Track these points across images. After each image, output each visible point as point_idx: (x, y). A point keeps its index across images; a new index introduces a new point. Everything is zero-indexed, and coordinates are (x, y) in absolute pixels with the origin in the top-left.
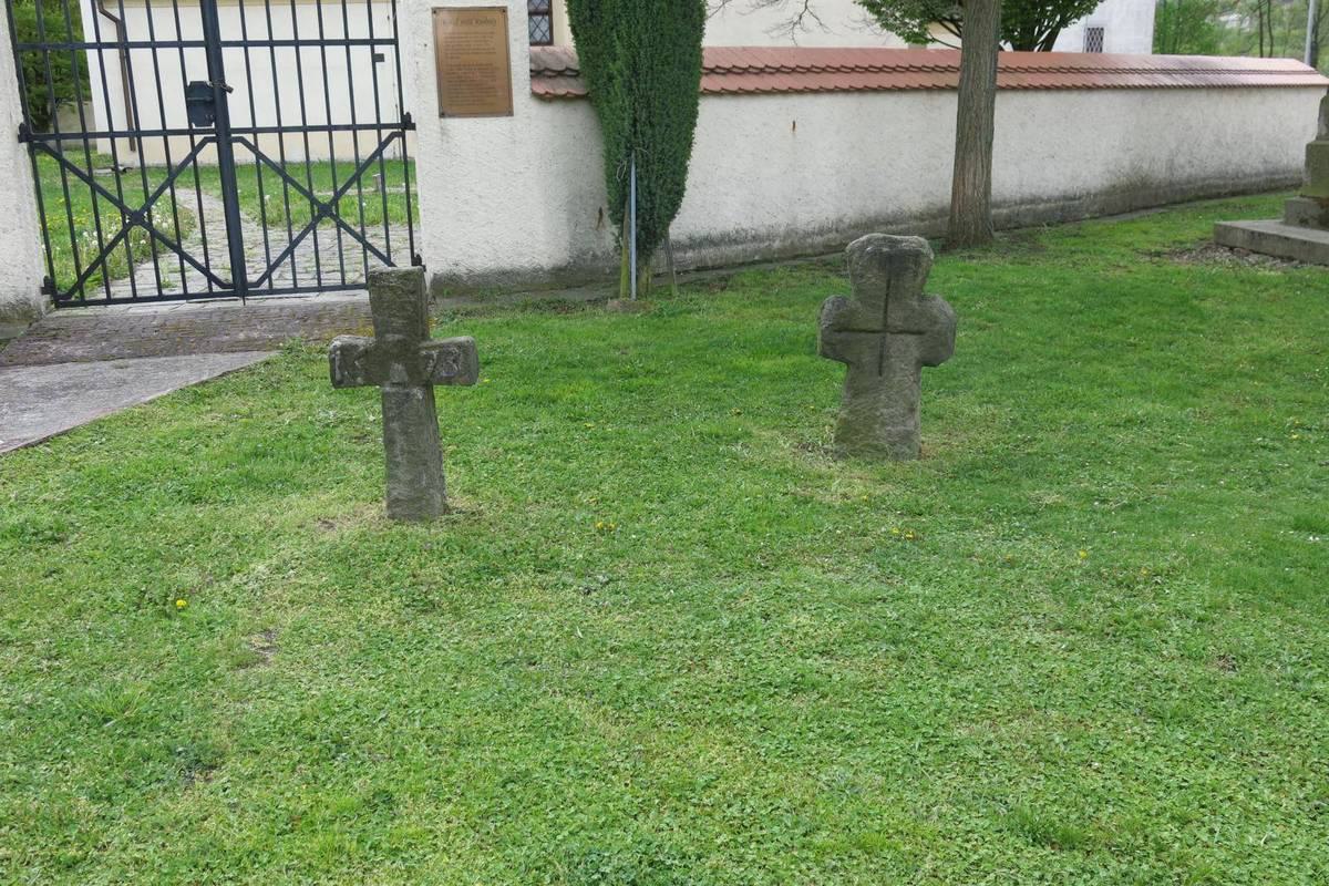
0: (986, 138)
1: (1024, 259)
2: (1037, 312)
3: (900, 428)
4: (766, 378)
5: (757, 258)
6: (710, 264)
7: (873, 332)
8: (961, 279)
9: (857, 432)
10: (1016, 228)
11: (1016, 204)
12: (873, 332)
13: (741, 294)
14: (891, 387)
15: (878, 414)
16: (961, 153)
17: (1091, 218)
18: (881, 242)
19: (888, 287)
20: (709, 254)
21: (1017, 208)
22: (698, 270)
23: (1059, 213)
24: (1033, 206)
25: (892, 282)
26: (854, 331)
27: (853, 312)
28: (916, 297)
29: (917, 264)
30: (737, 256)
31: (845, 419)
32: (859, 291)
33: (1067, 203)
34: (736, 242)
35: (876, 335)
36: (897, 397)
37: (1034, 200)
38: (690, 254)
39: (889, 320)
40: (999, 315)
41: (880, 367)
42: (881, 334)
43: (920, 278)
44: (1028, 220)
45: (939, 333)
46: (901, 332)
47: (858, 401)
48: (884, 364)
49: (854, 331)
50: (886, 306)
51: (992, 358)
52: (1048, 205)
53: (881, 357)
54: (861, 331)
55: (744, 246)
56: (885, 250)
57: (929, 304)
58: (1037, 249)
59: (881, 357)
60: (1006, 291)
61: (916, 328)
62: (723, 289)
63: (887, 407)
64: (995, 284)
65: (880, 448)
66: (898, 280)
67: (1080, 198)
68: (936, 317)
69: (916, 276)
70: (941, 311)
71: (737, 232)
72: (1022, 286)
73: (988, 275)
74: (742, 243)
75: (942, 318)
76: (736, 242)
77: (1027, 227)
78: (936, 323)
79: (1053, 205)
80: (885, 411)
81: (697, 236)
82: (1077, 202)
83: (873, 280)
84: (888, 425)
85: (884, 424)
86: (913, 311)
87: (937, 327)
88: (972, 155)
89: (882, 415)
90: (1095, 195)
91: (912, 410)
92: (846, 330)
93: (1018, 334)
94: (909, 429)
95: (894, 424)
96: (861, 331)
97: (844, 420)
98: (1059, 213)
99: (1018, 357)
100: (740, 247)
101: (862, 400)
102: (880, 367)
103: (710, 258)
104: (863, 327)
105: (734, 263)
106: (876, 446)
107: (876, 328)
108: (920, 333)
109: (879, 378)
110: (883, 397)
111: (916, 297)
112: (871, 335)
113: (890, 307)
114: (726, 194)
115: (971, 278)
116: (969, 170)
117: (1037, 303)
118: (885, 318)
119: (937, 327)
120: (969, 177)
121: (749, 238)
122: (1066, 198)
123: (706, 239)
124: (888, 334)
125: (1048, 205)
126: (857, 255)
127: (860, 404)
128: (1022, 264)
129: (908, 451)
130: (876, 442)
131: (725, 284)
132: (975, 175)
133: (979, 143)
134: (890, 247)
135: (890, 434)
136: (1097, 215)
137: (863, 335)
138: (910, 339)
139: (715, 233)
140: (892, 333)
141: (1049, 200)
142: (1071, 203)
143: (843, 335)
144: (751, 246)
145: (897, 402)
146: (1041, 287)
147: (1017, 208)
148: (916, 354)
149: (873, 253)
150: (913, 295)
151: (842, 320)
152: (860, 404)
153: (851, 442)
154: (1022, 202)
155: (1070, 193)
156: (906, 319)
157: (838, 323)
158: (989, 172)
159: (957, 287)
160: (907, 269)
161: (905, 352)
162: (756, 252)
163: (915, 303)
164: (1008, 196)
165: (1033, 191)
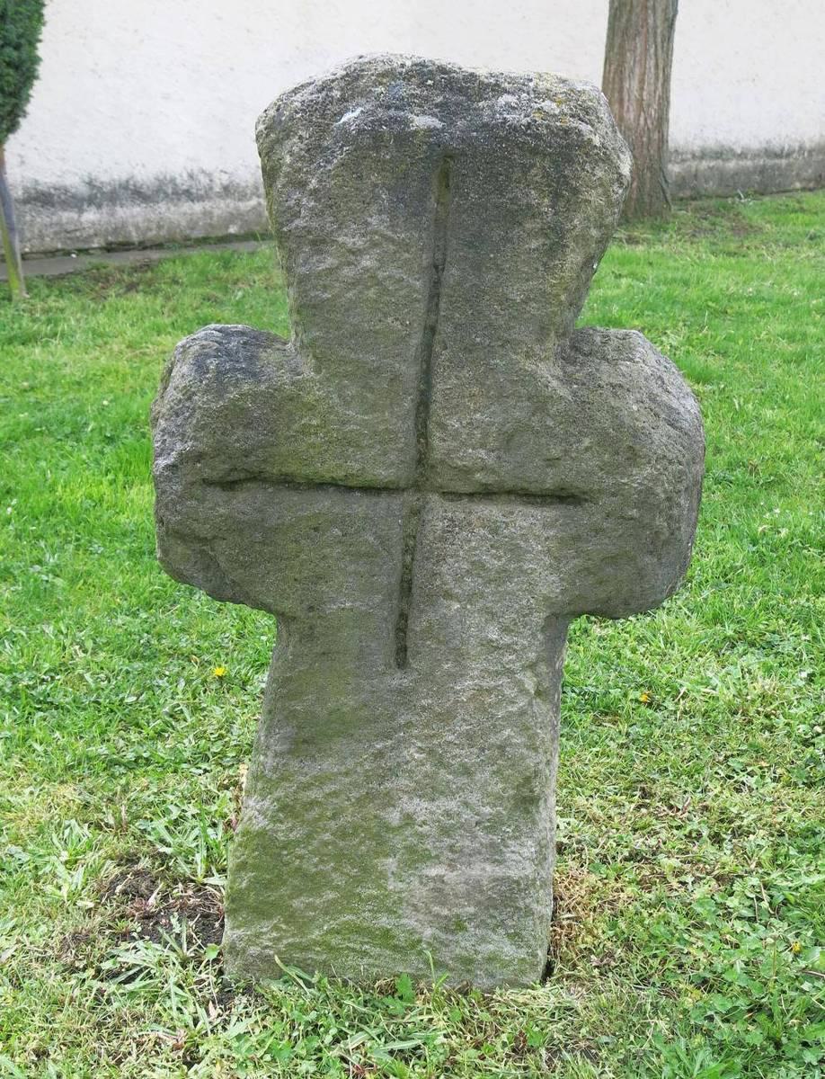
0: (665, 11)
1: (732, 247)
2: (800, 359)
3: (484, 871)
4: (122, 547)
5: (233, 230)
6: (135, 237)
7: (371, 489)
8: (624, 281)
9: (314, 883)
10: (694, 199)
11: (694, 156)
12: (371, 489)
13: (159, 300)
14: (446, 717)
15: (394, 817)
16: (618, 41)
17: (803, 189)
18: (405, 90)
19: (434, 296)
20: (133, 216)
21: (694, 164)
22: (109, 249)
23: (757, 178)
24: (720, 162)
25: (452, 273)
26: (288, 482)
27: (281, 404)
28: (552, 343)
29: (563, 191)
30: (193, 225)
31: (262, 834)
32: (308, 310)
33: (770, 162)
34: (189, 195)
35: (383, 501)
36: (469, 756)
37: (720, 154)
38: (90, 216)
39: (439, 444)
40: (715, 364)
41: (402, 629)
42: (410, 498)
43: (574, 258)
44: (711, 186)
45: (645, 499)
46: (487, 493)
47: (313, 769)
48: (418, 625)
49: (288, 482)
50: (427, 375)
51: (717, 481)
52: (742, 163)
53: (406, 587)
54: (321, 485)
55: (208, 205)
56: (421, 121)
57: (606, 374)
58: (744, 230)
59: (406, 587)
60: (719, 309)
61: (550, 481)
62: (131, 287)
63: (430, 790)
64: (693, 293)
65: (402, 938)
66: (478, 268)
67: (788, 155)
68: (635, 434)
69: (555, 248)
70: (655, 406)
71: (191, 176)
72: (750, 299)
73: (679, 275)
74: (200, 198)
75: (661, 436)
76: (189, 195)
77: (709, 197)
78: (634, 457)
79: (749, 163)
80: (419, 807)
81: (104, 178)
82: (784, 162)
83: (367, 262)
84: (426, 858)
85: (415, 857)
86: (540, 403)
87: (641, 475)
88: (639, 42)
89: (409, 819)
90: (810, 152)
91: (527, 802)
92: (256, 477)
93: (768, 414)
94: (514, 873)
95: (457, 857)
96: (321, 485)
97: (262, 842)
98: (757, 178)
99: (780, 481)
100: (198, 207)
101: (328, 765)
102: (402, 629)
103: (137, 227)
104: (329, 468)
105: (187, 239)
106: (387, 934)
107: (383, 474)
108: (563, 497)
109: (398, 680)
110: (413, 753)
111: (552, 343)
112: (360, 506)
113: (442, 386)
114: (166, 97)
115: (644, 280)
116: (632, 71)
117: (791, 338)
118: (422, 433)
119: (641, 475)
120: (632, 85)
121: (217, 189)
122: (769, 153)
123: (125, 186)
124: (434, 498)
125: (742, 163)
126: (294, 144)
127: (320, 781)
128: (729, 254)
129: (509, 950)
130: (384, 921)
131: (141, 280)
132: (642, 81)
133: (651, 21)
134: (445, 111)
135: (440, 892)
136: (811, 185)
137: (325, 503)
138: (527, 521)
139: (145, 175)
140: (452, 495)
141: (742, 156)
142: (777, 161)
143: (244, 503)
144: (221, 207)
145: (467, 771)
146: (787, 302)
147: (694, 164)
148: (549, 584)
149: (371, 140)
150: (543, 333)
151: (238, 439)
152: (320, 781)
153: (291, 918)
154: (703, 155)
155: (776, 145)
156: (508, 441)
157: (219, 450)
158: (667, 80)
159: (618, 297)
160: (514, 216)
161: (503, 576)
162: (232, 218)
163: (548, 372)
164: (682, 143)
165: (720, 137)
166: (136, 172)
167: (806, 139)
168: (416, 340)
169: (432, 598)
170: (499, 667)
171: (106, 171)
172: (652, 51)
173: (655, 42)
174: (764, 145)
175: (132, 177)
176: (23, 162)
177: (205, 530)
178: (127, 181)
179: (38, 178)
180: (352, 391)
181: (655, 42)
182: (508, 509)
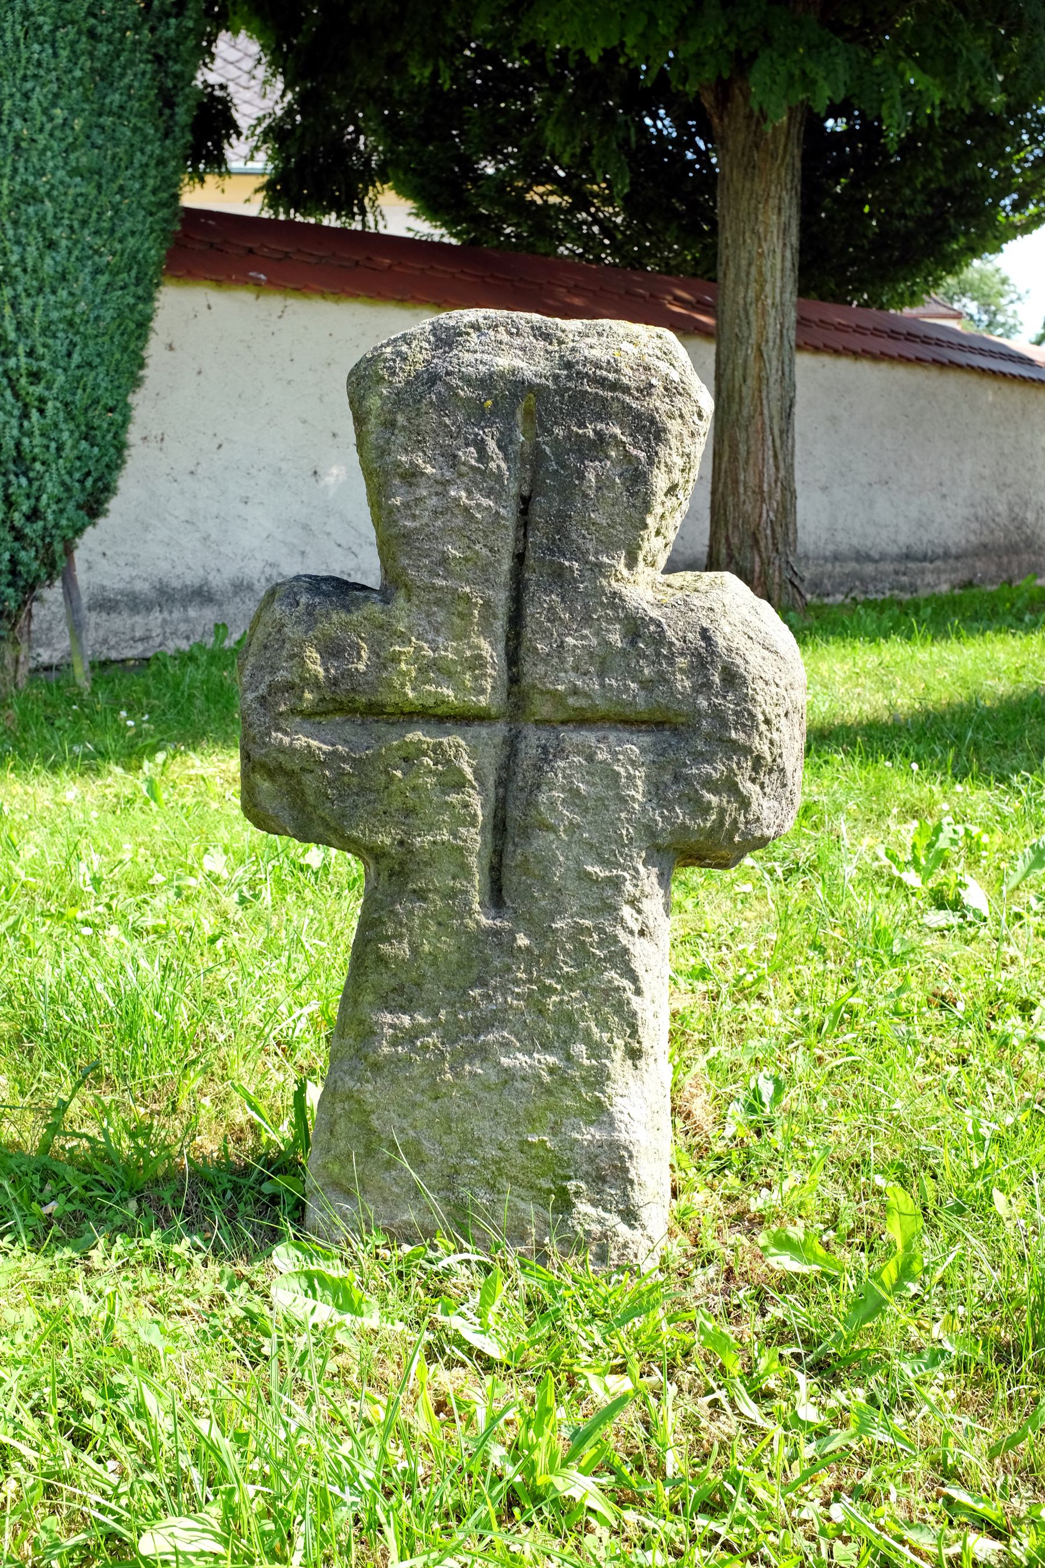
48: (514, 859)
113: (535, 613)
133: (766, 412)
165: (855, 542)
166: (210, 578)
167: (950, 544)
168: (506, 565)
169: (526, 833)
170: (598, 903)
171: (178, 577)
172: (770, 443)
173: (772, 434)
174: (904, 550)
175: (206, 583)
176: (90, 568)
177: (295, 765)
178: (201, 587)
179: (105, 583)
180: (440, 617)
181: (772, 434)
182: (600, 734)
